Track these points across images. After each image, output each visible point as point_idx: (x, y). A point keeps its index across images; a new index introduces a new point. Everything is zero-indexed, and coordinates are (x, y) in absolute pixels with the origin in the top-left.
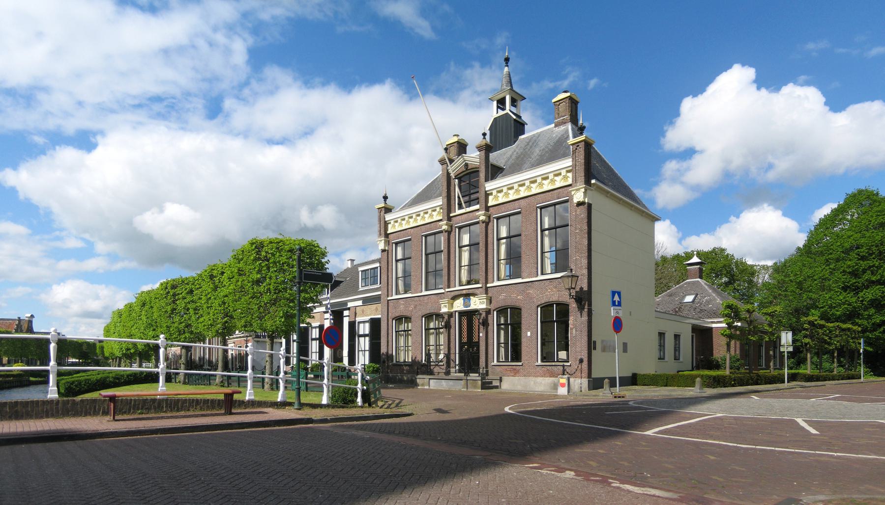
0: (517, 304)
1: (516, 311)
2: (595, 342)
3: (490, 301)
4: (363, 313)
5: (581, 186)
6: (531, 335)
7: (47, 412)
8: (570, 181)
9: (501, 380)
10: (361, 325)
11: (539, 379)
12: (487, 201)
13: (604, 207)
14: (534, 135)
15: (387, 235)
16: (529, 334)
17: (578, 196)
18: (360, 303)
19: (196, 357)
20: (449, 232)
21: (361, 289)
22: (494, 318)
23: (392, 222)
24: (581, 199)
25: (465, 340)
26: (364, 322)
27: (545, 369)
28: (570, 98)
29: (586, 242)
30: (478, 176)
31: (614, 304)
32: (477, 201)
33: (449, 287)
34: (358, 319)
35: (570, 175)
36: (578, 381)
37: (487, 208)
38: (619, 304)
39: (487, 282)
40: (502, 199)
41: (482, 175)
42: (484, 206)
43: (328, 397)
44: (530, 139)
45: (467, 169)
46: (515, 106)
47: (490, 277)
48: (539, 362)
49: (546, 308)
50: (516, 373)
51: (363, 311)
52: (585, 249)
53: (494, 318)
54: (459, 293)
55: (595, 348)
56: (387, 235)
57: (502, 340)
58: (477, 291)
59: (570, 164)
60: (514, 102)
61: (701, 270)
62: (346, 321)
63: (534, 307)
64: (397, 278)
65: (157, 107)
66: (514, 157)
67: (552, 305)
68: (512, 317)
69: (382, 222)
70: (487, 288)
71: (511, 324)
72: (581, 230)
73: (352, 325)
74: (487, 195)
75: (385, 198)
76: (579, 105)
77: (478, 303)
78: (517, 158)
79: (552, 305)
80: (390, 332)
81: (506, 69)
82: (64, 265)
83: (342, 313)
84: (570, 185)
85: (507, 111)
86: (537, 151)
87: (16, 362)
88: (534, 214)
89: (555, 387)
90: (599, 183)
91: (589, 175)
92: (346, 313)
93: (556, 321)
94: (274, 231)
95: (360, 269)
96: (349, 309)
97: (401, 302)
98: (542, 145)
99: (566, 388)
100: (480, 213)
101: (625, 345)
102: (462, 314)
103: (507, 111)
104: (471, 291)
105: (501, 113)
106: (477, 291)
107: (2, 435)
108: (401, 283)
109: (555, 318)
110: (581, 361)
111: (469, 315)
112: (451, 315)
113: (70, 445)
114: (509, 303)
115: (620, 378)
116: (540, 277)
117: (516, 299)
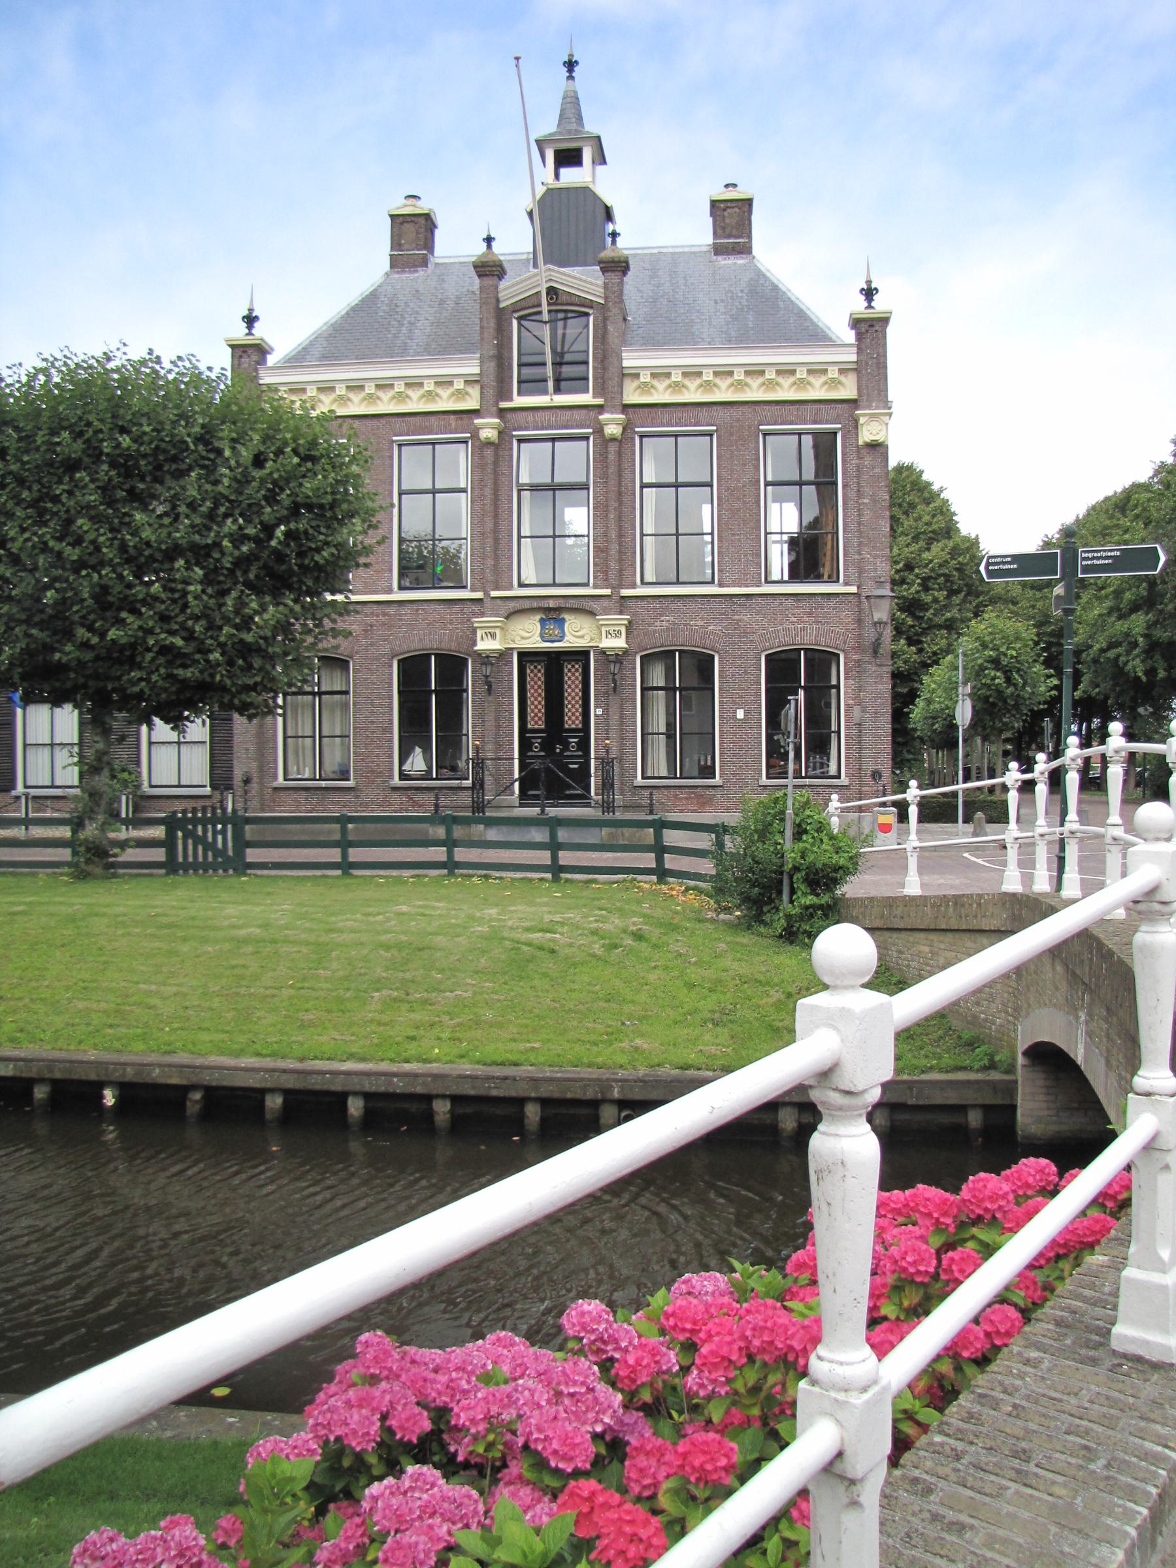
19: (417, 1358)
25: (537, 721)
40: (661, 395)
48: (764, 780)
54: (527, 604)
58: (595, 606)
59: (477, 370)
65: (570, 113)
67: (428, 656)
71: (681, 689)
72: (874, 501)
79: (428, 656)
82: (135, 1262)
84: (853, 403)
93: (681, 689)
94: (346, 609)
97: (406, 609)
102: (526, 657)
111: (553, 665)
114: (684, 640)
115: (956, 821)
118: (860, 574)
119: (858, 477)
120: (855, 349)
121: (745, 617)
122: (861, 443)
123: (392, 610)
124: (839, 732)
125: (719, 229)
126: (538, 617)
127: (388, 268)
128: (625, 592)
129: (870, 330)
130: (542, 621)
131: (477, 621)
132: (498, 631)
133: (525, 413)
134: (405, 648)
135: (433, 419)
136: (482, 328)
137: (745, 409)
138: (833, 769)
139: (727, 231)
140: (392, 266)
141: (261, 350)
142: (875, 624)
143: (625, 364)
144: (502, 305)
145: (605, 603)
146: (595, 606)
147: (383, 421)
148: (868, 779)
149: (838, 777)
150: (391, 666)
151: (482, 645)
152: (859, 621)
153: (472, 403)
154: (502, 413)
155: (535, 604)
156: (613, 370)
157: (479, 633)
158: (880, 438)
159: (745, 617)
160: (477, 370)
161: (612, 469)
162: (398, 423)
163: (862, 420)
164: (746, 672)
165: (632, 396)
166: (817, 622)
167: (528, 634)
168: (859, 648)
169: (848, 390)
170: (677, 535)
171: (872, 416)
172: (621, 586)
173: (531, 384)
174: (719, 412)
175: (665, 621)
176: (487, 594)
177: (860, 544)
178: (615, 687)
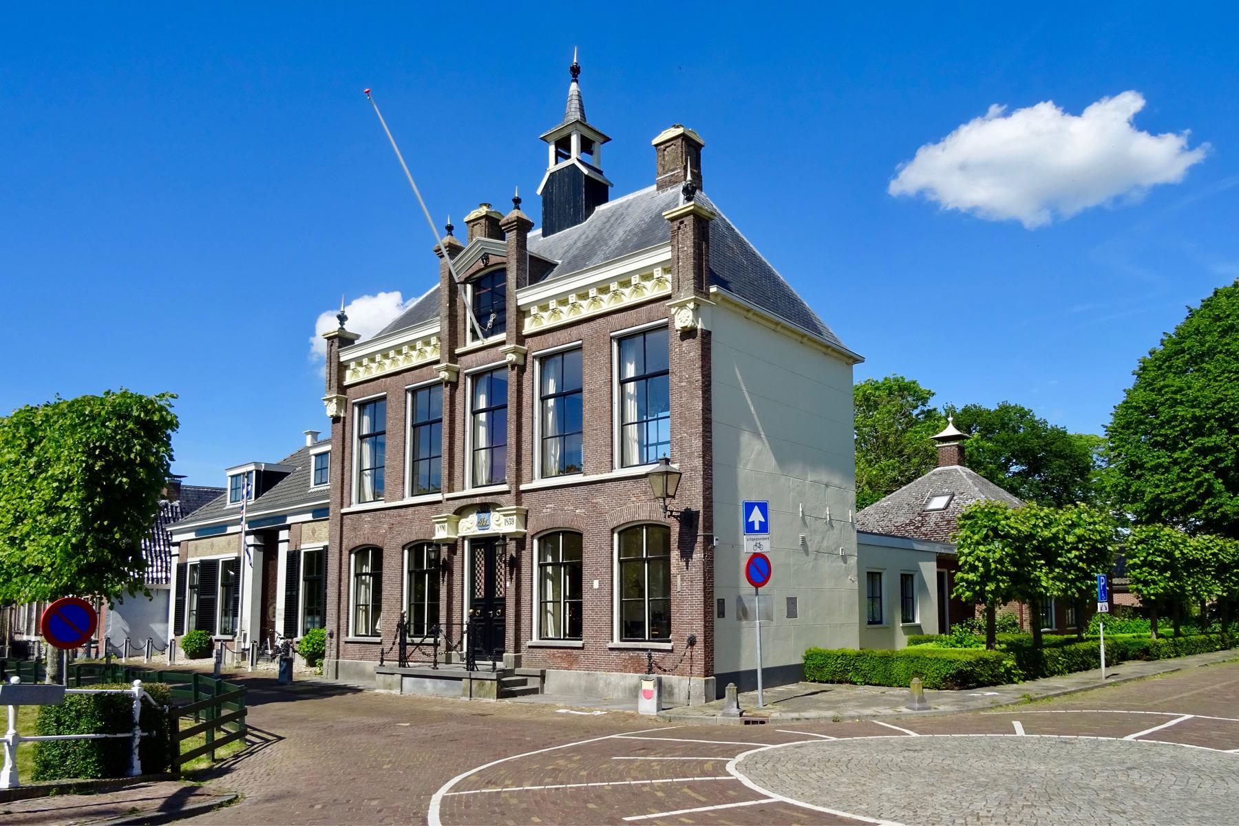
0: (577, 525)
1: (574, 539)
2: (721, 603)
3: (525, 517)
5: (687, 295)
8: (668, 290)
9: (543, 676)
11: (615, 677)
12: (520, 326)
13: (744, 341)
14: (621, 205)
15: (343, 389)
16: (596, 584)
17: (683, 319)
18: (309, 517)
20: (454, 385)
21: (313, 488)
22: (533, 555)
23: (353, 365)
24: (689, 323)
25: (480, 594)
27: (624, 655)
28: (683, 136)
29: (698, 405)
30: (505, 280)
31: (750, 528)
32: (499, 326)
33: (451, 490)
35: (669, 277)
36: (685, 681)
37: (521, 339)
38: (764, 528)
39: (519, 480)
41: (511, 277)
42: (514, 334)
44: (614, 212)
45: (486, 266)
46: (591, 153)
47: (346, 500)
48: (616, 642)
50: (571, 663)
51: (314, 532)
52: (698, 419)
53: (533, 555)
54: (469, 501)
55: (721, 614)
56: (343, 389)
57: (550, 597)
59: (668, 256)
60: (586, 146)
61: (961, 449)
62: (283, 550)
63: (607, 533)
64: (361, 471)
66: (579, 244)
68: (565, 548)
69: (334, 365)
70: (519, 493)
74: (522, 313)
76: (702, 151)
77: (501, 523)
78: (585, 246)
80: (344, 576)
81: (574, 86)
83: (277, 536)
84: (668, 297)
85: (573, 160)
86: (620, 233)
88: (607, 351)
89: (635, 692)
90: (724, 292)
91: (706, 274)
92: (283, 535)
93: (649, 561)
95: (313, 452)
96: (288, 527)
97: (366, 517)
98: (630, 223)
99: (654, 701)
100: (507, 347)
101: (792, 602)
102: (476, 542)
103: (573, 160)
104: (489, 499)
105: (564, 164)
106: (501, 499)
108: (368, 481)
109: (645, 550)
110: (692, 642)
111: (486, 545)
112: (453, 546)
114: (561, 522)
116: (619, 472)
117: (569, 513)
143: (342, 359)
150: (403, 554)
164: (601, 548)
167: (470, 526)
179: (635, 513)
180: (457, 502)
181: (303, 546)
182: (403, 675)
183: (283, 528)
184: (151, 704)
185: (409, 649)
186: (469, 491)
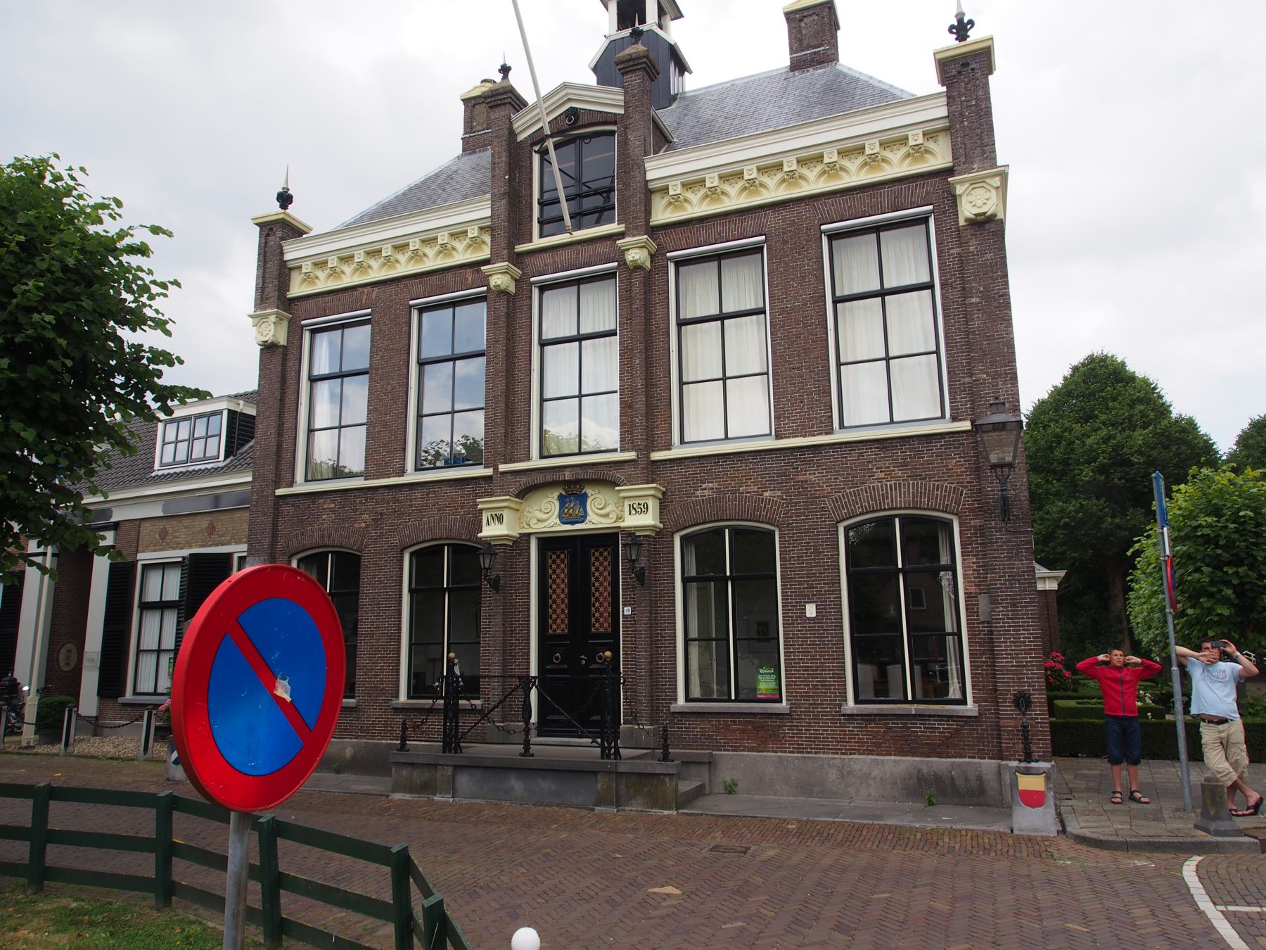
1: (754, 546)
4: (164, 541)
6: (813, 607)
7: (376, 410)
10: (154, 579)
11: (861, 762)
25: (560, 626)
26: (163, 566)
34: (144, 557)
40: (697, 207)
43: (172, 676)
49: (870, 548)
51: (163, 534)
54: (540, 479)
69: (273, 266)
73: (122, 578)
75: (285, 199)
84: (949, 172)
87: (668, 884)
96: (116, 526)
102: (549, 544)
107: (5, 781)
111: (576, 554)
113: (312, 301)
118: (973, 402)
119: (961, 270)
120: (944, 100)
121: (812, 477)
122: (962, 222)
123: (402, 495)
124: (687, 641)
125: (797, 40)
126: (556, 494)
127: (460, 151)
128: (656, 456)
129: (966, 71)
130: (561, 498)
131: (482, 503)
132: (505, 513)
133: (543, 255)
134: (428, 535)
135: (449, 276)
136: (493, 164)
137: (802, 208)
138: (954, 692)
139: (805, 43)
140: (464, 150)
141: (294, 231)
142: (994, 467)
144: (521, 138)
145: (629, 470)
146: (619, 474)
147: (401, 285)
148: (1007, 707)
149: (963, 701)
150: (401, 561)
151: (490, 530)
152: (977, 470)
153: (485, 253)
154: (517, 259)
155: (549, 478)
156: (636, 185)
157: (485, 516)
158: (989, 208)
159: (812, 477)
160: (488, 213)
161: (638, 303)
162: (415, 286)
163: (959, 190)
164: (817, 552)
165: (662, 214)
166: (913, 477)
167: (544, 515)
168: (981, 510)
169: (940, 157)
170: (724, 379)
171: (973, 182)
172: (653, 448)
173: (551, 223)
174: (771, 219)
175: (706, 491)
176: (496, 469)
177: (970, 361)
178: (649, 580)
179: (885, 497)
180: (524, 479)
181: (140, 556)
182: (457, 768)
183: (106, 528)
184: (655, 887)
185: (465, 723)
186: (536, 462)
